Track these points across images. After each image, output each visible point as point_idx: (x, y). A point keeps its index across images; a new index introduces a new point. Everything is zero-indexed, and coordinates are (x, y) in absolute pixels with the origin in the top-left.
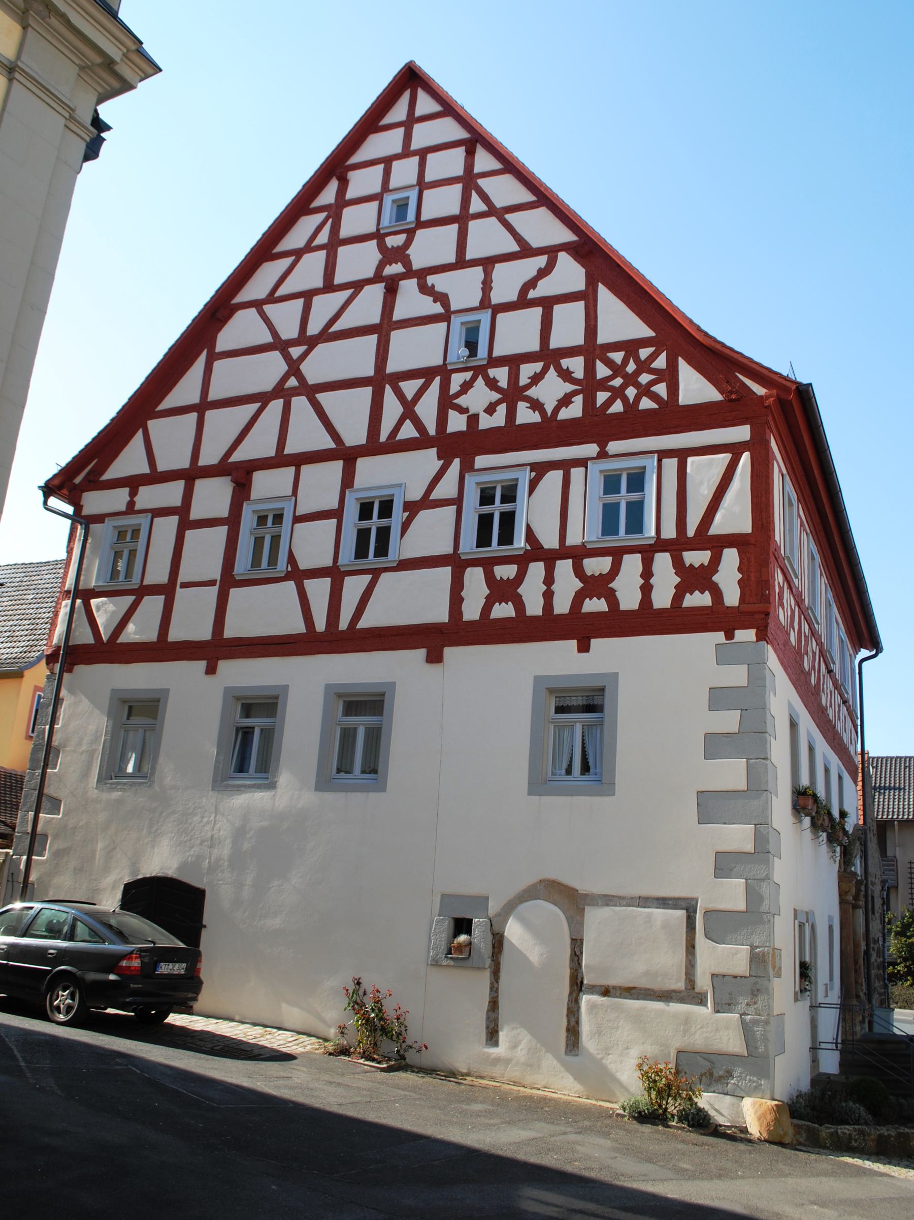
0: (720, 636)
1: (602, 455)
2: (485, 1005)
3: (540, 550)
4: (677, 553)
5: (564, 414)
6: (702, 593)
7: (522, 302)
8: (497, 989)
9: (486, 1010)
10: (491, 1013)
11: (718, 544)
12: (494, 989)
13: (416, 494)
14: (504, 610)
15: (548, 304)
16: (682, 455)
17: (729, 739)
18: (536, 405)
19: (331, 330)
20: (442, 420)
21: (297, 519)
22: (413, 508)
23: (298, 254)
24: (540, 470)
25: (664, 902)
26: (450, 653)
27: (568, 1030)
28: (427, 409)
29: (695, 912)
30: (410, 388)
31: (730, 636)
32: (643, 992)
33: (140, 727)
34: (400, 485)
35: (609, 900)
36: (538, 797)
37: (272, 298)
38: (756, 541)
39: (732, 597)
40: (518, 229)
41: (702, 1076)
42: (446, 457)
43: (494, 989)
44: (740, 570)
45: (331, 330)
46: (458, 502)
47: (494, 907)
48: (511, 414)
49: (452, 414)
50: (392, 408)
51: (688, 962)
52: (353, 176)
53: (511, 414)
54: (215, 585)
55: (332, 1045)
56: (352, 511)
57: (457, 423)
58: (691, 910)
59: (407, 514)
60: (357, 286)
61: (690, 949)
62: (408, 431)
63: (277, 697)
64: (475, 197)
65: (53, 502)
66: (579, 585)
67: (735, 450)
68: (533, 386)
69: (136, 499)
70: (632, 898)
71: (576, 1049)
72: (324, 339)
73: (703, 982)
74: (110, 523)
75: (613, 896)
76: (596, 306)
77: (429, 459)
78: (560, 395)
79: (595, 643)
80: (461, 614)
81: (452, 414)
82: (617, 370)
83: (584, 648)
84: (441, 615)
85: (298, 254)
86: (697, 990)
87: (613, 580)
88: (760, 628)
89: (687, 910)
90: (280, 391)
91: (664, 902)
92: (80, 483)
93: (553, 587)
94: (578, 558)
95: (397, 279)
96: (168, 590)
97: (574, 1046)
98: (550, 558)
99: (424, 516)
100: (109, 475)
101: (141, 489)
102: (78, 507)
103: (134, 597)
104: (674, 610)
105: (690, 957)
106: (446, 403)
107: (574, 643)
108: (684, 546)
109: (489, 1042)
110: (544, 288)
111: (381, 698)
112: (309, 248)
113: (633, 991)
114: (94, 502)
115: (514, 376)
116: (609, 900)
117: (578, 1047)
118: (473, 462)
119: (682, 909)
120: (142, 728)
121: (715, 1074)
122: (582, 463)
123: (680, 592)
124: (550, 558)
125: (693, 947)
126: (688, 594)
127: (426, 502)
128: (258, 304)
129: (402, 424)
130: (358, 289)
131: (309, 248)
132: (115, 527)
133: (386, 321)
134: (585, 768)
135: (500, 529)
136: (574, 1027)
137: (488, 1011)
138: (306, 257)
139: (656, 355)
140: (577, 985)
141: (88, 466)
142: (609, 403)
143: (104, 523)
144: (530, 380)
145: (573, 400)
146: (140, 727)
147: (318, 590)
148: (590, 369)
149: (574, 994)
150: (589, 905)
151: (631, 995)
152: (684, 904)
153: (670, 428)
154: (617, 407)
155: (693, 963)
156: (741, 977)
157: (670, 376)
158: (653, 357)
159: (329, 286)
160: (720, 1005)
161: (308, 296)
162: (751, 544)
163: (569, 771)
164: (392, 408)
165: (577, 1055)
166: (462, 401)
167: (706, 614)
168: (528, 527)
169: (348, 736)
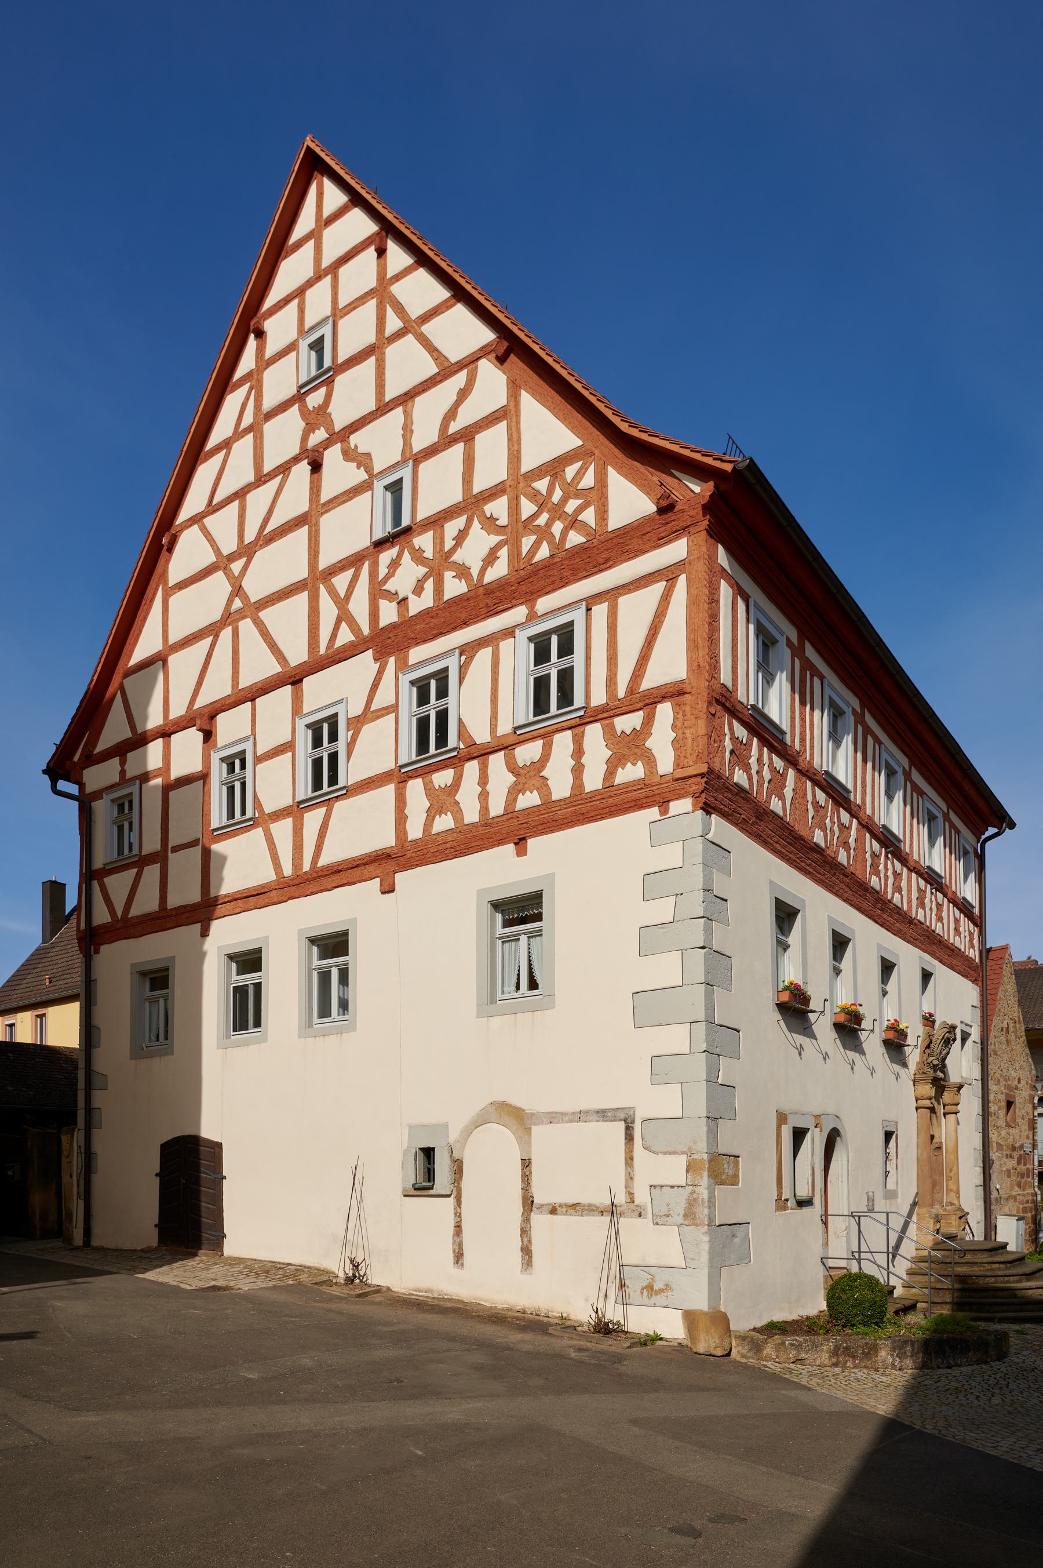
0: (654, 812)
1: (532, 617)
2: (451, 1231)
3: (473, 747)
4: (607, 722)
5: (491, 576)
6: (634, 764)
7: (446, 441)
8: (460, 1214)
9: (452, 1235)
10: (456, 1238)
11: (649, 701)
12: (458, 1215)
13: (356, 708)
14: (631, 773)
15: (467, 435)
16: (611, 596)
17: (665, 930)
18: (463, 572)
19: (265, 532)
20: (374, 614)
21: (259, 760)
22: (357, 723)
23: (226, 445)
24: (469, 650)
25: (603, 1115)
26: (401, 878)
27: (522, 1249)
28: (359, 606)
29: (633, 1122)
30: (341, 581)
31: (664, 811)
32: (586, 1208)
33: (159, 997)
34: (341, 701)
35: (553, 1118)
36: (303, 1039)
37: (212, 508)
38: (692, 688)
39: (665, 764)
40: (437, 343)
41: (643, 1289)
42: (380, 657)
43: (458, 1215)
44: (674, 727)
45: (265, 532)
46: (394, 708)
47: (453, 1136)
48: (439, 590)
49: (383, 604)
50: (328, 610)
51: (628, 1174)
52: (268, 325)
53: (439, 590)
54: (197, 845)
55: (906, 1381)
56: (304, 739)
57: (388, 614)
58: (629, 1120)
59: (350, 733)
60: (284, 469)
61: (629, 1161)
62: (345, 636)
63: (167, 969)
64: (390, 313)
65: (63, 785)
66: (511, 779)
67: (668, 575)
68: (457, 549)
69: (127, 767)
70: (574, 1113)
71: (529, 1267)
72: (261, 545)
73: (642, 1196)
74: (107, 798)
75: (556, 1113)
76: (518, 423)
77: (365, 663)
78: (485, 552)
79: (531, 842)
80: (406, 834)
81: (383, 604)
82: (542, 503)
83: (521, 850)
84: (387, 840)
85: (226, 445)
86: (637, 1202)
87: (543, 767)
88: (696, 795)
89: (625, 1121)
90: (229, 618)
91: (603, 1115)
92: (79, 760)
93: (489, 787)
94: (509, 748)
95: (321, 450)
96: (160, 857)
97: (528, 1265)
98: (482, 753)
99: (368, 731)
100: (101, 746)
101: (129, 755)
102: (82, 786)
103: (136, 870)
104: (606, 790)
105: (630, 1170)
106: (378, 592)
107: (511, 847)
108: (614, 711)
109: (456, 1265)
110: (465, 417)
111: (257, 955)
112: (238, 434)
113: (578, 1208)
114: (98, 776)
115: (439, 541)
116: (553, 1118)
117: (532, 1266)
118: (406, 659)
119: (621, 1120)
120: (163, 997)
121: (656, 1288)
122: (509, 632)
123: (613, 766)
124: (482, 753)
125: (632, 1159)
126: (620, 769)
127: (368, 715)
128: (197, 519)
129: (338, 629)
130: (287, 473)
131: (238, 434)
132: (113, 801)
133: (314, 506)
134: (533, 985)
135: (437, 732)
136: (527, 1247)
137: (454, 1235)
138: (236, 447)
139: (583, 471)
140: (528, 1204)
141: (77, 750)
142: (536, 546)
143: (102, 798)
144: (455, 542)
145: (498, 555)
146: (159, 997)
147: (282, 830)
148: (514, 509)
149: (526, 1214)
150: (535, 1124)
151: (576, 1212)
152: (623, 1116)
153: (600, 565)
154: (544, 552)
155: (632, 1175)
156: (678, 1186)
157: (599, 495)
158: (580, 474)
159: (261, 479)
160: (659, 1217)
161: (240, 495)
162: (686, 693)
163: (518, 988)
164: (328, 610)
165: (532, 1274)
166: (390, 586)
167: (639, 789)
168: (460, 720)
169: (325, 977)
